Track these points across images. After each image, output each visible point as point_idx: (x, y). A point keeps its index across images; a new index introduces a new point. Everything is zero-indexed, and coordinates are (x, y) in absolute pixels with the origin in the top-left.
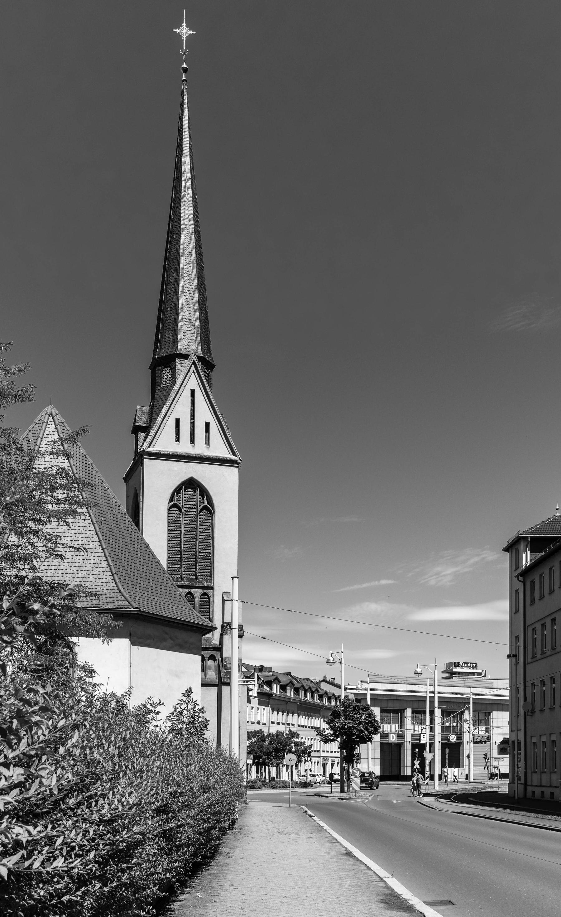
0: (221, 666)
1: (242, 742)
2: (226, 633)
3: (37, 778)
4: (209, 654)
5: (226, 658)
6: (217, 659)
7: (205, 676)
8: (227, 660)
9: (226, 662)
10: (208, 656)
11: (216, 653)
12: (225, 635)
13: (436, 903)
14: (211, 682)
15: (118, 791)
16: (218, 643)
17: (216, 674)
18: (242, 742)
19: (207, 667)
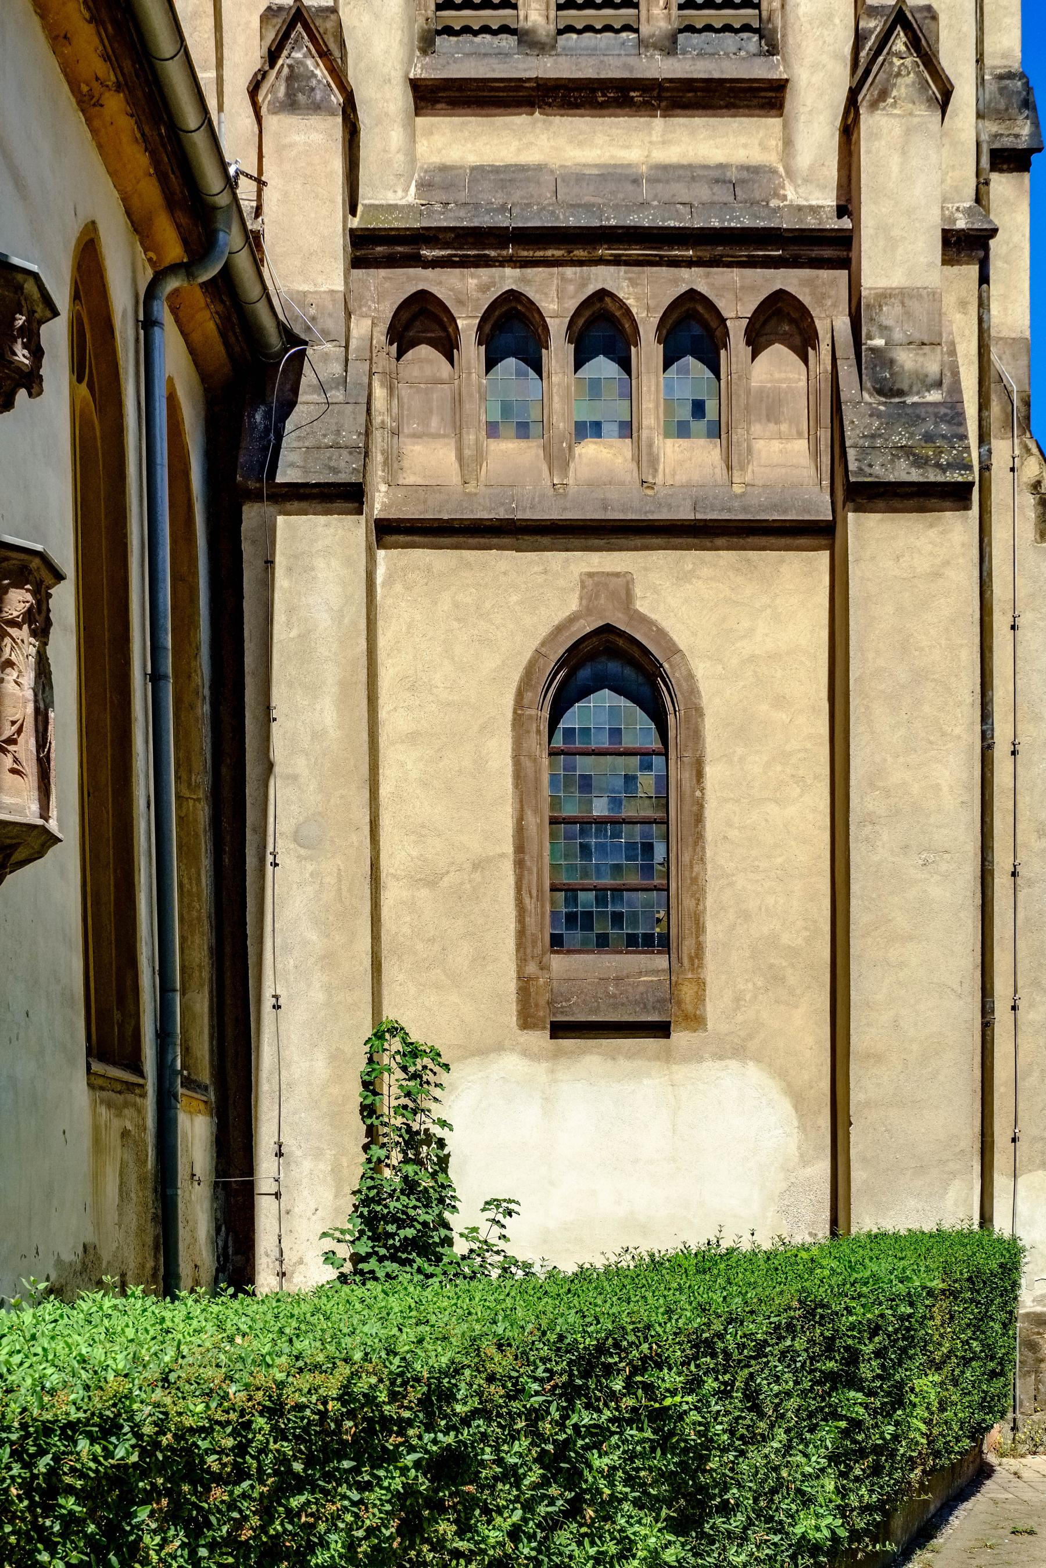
0: (847, 371)
1: (1036, 983)
2: (884, 95)
3: (362, 1270)
4: (753, 289)
5: (885, 296)
6: (822, 327)
7: (729, 468)
8: (889, 315)
9: (884, 329)
10: (748, 309)
11: (810, 283)
12: (874, 105)
13: (849, 192)
14: (775, 507)
15: (696, 1408)
16: (828, 200)
17: (815, 453)
18: (1036, 983)
19: (739, 401)
